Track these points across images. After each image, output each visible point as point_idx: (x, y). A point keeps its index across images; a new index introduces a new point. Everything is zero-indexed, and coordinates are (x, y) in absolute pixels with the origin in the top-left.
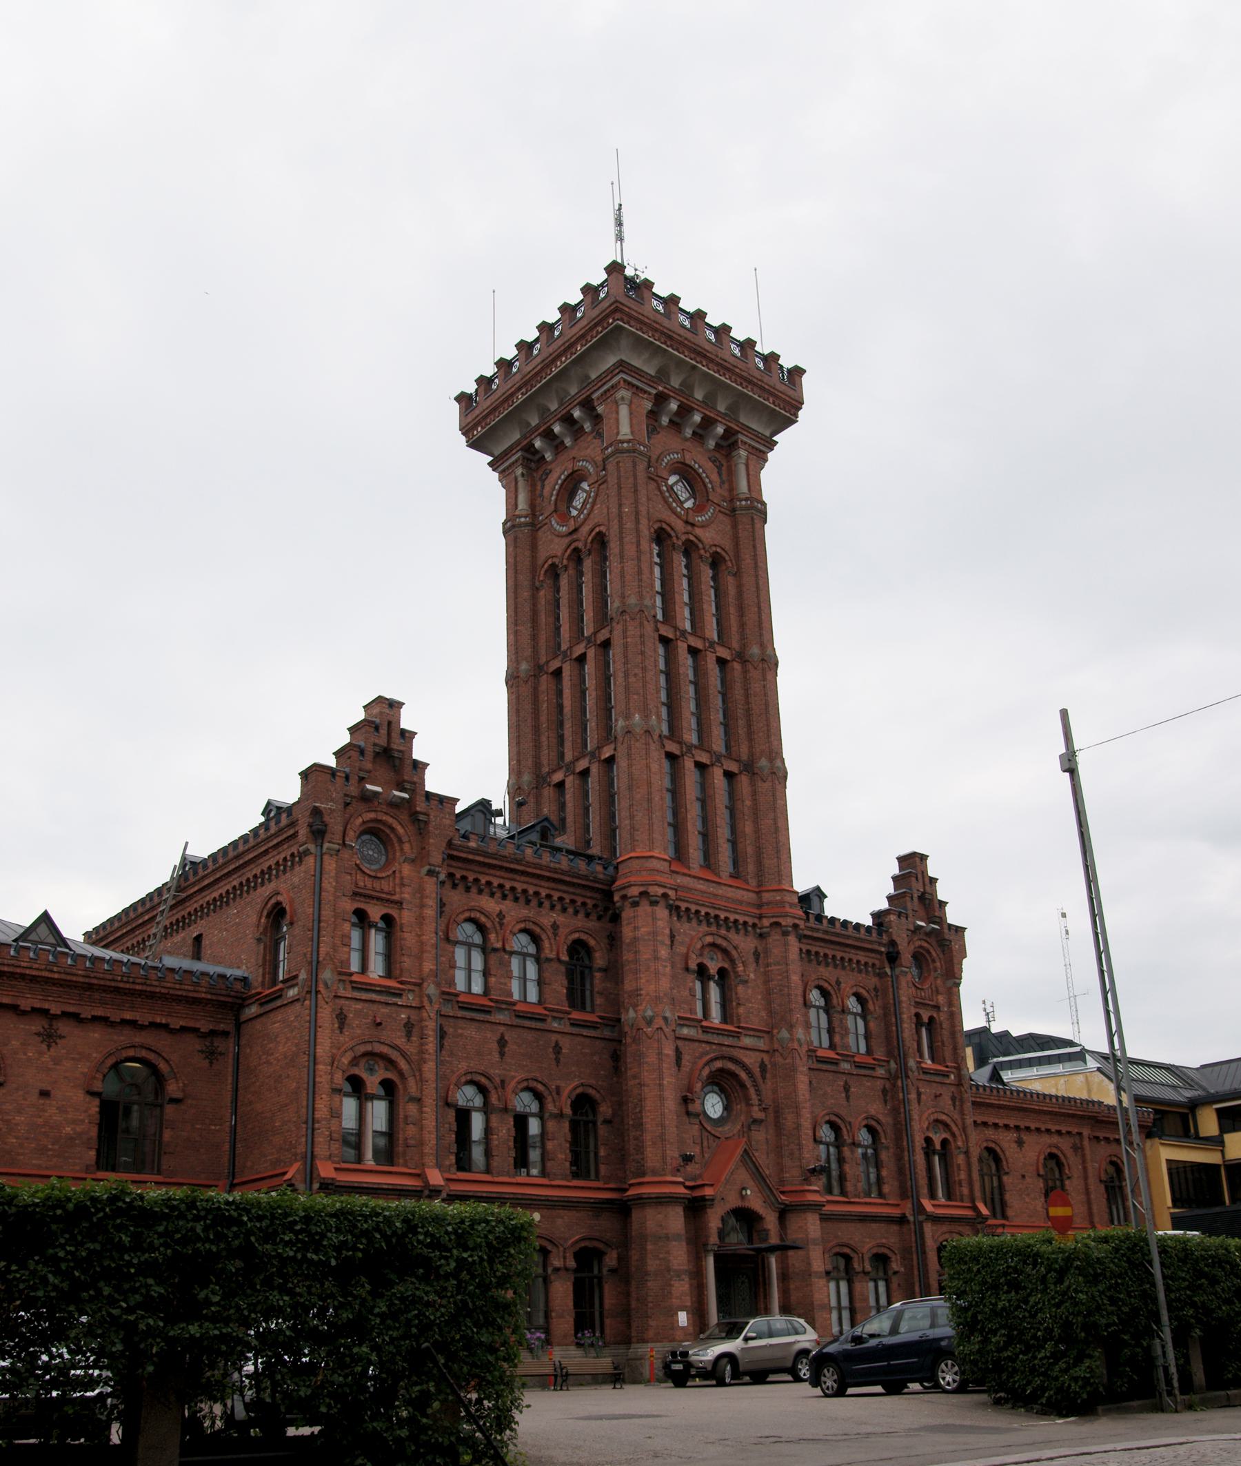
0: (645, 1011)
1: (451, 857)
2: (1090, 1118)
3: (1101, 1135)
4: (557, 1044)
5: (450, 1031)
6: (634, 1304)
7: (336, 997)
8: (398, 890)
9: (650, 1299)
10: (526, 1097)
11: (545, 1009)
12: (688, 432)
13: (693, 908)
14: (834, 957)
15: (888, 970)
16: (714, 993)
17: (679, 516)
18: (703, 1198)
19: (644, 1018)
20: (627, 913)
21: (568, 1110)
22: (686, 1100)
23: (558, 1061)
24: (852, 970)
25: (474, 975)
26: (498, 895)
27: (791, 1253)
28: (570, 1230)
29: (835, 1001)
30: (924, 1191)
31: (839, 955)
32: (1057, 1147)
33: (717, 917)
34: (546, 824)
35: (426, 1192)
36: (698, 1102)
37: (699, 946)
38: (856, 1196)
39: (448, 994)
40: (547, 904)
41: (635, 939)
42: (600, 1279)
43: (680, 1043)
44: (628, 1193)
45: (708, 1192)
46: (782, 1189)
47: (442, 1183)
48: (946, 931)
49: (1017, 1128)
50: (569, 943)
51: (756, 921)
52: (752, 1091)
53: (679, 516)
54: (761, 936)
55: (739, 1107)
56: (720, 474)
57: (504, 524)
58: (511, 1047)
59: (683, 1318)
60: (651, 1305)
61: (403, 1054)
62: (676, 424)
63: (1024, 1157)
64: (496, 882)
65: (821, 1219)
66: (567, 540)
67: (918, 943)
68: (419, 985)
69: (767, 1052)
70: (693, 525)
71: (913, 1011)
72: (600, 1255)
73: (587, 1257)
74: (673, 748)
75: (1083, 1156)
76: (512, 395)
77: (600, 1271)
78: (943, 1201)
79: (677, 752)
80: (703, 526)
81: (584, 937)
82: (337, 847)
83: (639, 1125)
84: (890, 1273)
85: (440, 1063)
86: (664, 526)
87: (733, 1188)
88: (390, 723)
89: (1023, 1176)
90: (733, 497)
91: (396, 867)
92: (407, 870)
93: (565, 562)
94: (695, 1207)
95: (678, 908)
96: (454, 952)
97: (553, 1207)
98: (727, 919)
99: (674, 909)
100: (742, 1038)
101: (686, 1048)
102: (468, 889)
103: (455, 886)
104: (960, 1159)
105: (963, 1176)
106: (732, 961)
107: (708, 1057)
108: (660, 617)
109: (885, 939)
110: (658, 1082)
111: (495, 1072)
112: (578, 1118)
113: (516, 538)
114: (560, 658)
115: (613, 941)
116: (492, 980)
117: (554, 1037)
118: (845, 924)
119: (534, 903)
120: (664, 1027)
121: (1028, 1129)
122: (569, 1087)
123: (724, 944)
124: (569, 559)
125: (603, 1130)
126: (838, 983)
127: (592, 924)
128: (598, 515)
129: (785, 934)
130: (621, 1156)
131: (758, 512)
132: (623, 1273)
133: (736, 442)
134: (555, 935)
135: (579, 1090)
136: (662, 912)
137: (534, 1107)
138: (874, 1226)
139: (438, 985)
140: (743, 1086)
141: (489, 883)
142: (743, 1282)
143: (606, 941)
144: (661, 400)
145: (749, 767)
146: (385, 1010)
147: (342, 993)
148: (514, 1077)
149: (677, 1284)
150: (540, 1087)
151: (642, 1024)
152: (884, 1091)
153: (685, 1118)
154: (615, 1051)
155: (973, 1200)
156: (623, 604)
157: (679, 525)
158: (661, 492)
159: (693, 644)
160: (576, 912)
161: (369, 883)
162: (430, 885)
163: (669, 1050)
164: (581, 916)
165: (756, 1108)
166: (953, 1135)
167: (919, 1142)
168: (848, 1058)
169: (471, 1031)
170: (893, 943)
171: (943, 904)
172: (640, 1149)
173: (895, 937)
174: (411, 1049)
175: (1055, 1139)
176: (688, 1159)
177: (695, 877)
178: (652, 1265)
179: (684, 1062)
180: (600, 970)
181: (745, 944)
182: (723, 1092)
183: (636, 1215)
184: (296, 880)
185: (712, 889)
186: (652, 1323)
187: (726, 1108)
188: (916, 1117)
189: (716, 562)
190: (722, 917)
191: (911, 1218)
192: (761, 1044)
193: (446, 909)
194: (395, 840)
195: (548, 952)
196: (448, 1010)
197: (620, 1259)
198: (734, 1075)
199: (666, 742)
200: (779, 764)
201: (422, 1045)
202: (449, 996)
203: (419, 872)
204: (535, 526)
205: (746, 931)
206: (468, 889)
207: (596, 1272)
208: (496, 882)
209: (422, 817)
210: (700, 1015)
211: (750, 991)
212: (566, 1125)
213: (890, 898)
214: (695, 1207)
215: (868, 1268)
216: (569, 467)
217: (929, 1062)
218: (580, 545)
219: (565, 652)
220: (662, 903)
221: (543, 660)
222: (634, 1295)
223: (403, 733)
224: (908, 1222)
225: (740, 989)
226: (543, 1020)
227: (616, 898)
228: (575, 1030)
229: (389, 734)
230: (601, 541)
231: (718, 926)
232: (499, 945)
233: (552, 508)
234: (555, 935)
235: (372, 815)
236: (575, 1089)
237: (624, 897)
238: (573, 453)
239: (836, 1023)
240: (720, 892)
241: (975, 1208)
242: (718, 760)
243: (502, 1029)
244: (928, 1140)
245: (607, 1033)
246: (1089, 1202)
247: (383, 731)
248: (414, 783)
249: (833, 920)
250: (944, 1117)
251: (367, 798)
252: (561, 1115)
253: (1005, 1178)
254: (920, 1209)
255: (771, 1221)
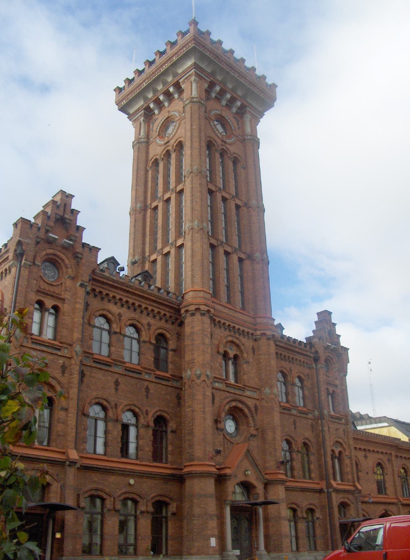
0: (196, 371)
1: (94, 280)
2: (396, 446)
3: (399, 455)
4: (147, 387)
5: (87, 373)
6: (185, 533)
7: (22, 346)
8: (63, 293)
9: (195, 530)
10: (129, 415)
11: (142, 367)
12: (224, 103)
13: (222, 321)
14: (289, 357)
15: (314, 366)
16: (231, 368)
17: (219, 138)
18: (225, 475)
19: (196, 375)
20: (188, 320)
21: (152, 424)
22: (216, 421)
23: (147, 396)
24: (297, 365)
25: (103, 345)
26: (119, 304)
27: (270, 506)
28: (151, 490)
29: (289, 379)
30: (331, 476)
31: (291, 356)
32: (381, 460)
33: (234, 327)
34: (146, 274)
35: (68, 463)
36: (223, 423)
37: (225, 341)
38: (300, 478)
39: (88, 353)
40: (145, 312)
41: (192, 333)
42: (166, 518)
43: (214, 391)
44: (184, 471)
45: (228, 471)
46: (266, 472)
47: (77, 458)
48: (340, 349)
49: (365, 450)
50: (156, 334)
51: (254, 332)
52: (250, 419)
53: (219, 138)
54: (256, 340)
55: (243, 427)
56: (238, 124)
57: (133, 142)
58: (121, 387)
59: (213, 542)
60: (195, 534)
61: (59, 383)
62: (218, 99)
63: (369, 463)
64: (118, 297)
65: (286, 490)
66: (163, 147)
67: (328, 354)
68: (71, 345)
69: (258, 400)
70: (225, 142)
71: (326, 386)
72: (167, 504)
73: (160, 505)
74: (214, 242)
75: (392, 464)
76: (141, 84)
77: (166, 513)
78: (340, 482)
79: (216, 244)
80: (230, 144)
81: (164, 332)
82: (29, 263)
83: (191, 433)
84: (315, 518)
85: (80, 391)
86: (212, 140)
87: (240, 469)
88: (65, 205)
89: (367, 473)
90: (244, 134)
91: (63, 281)
92: (69, 283)
93: (162, 157)
94: (221, 479)
95: (214, 320)
96: (92, 331)
97: (142, 477)
98: (239, 329)
99: (213, 320)
100: (246, 391)
101: (218, 394)
102: (102, 299)
103: (95, 296)
104: (347, 461)
105: (349, 469)
106: (241, 351)
107: (228, 400)
108: (210, 234)
109: (313, 350)
110: (200, 410)
111: (113, 400)
112: (157, 428)
113: (139, 148)
114: (157, 201)
115: (180, 336)
116: (113, 349)
117: (146, 383)
118: (295, 340)
119: (138, 311)
120: (206, 380)
121: (369, 450)
122: (153, 412)
123: (238, 342)
124: (164, 155)
125: (170, 436)
126: (291, 370)
127: (169, 326)
128: (181, 132)
129: (269, 339)
130: (180, 450)
131: (256, 143)
132: (178, 515)
133: (246, 111)
134: (149, 329)
135: (158, 413)
136: (207, 320)
137: (133, 421)
138: (308, 494)
139: (82, 346)
140: (246, 417)
141: (114, 297)
142: (245, 522)
143: (176, 336)
144: (212, 85)
145: (250, 257)
146: (51, 357)
147: (25, 344)
148: (123, 403)
149: (210, 522)
150: (137, 410)
151: (195, 378)
152: (312, 426)
153: (216, 431)
154: (178, 394)
155: (354, 482)
156: (192, 169)
157: (219, 142)
158: (211, 125)
159: (224, 195)
160: (161, 319)
161: (47, 287)
162: (81, 293)
163: (209, 393)
164: (163, 321)
165: (252, 429)
166: (344, 449)
167: (329, 453)
168: (296, 407)
169: (99, 375)
170: (316, 352)
171: (339, 336)
172: (191, 446)
173: (318, 350)
174: (64, 380)
175: (380, 456)
176: (218, 452)
177: (223, 306)
178: (197, 511)
179: (216, 401)
180: (172, 350)
181: (247, 343)
182: (235, 419)
183: (188, 483)
184: (6, 283)
185: (232, 313)
186: (196, 544)
187: (236, 429)
188: (328, 439)
189: (235, 161)
190: (237, 328)
191: (326, 490)
192: (255, 395)
193: (90, 308)
194: (63, 266)
195: (144, 337)
196: (89, 362)
197: (177, 507)
198: (241, 410)
199: (210, 238)
200: (265, 256)
201: (70, 378)
202: (88, 354)
203: (76, 285)
204: (148, 143)
205: (248, 335)
206: (102, 299)
207: (164, 514)
208: (118, 297)
209: (79, 255)
210: (224, 377)
211: (250, 368)
212: (151, 432)
213: (314, 331)
214: (221, 479)
215: (305, 516)
216: (166, 115)
217: (333, 412)
218: (170, 148)
219: (160, 197)
220: (207, 315)
221: (147, 254)
222: (185, 528)
223: (73, 211)
224: (324, 492)
225: (245, 366)
226: (140, 373)
227: (183, 311)
228: (158, 381)
229: (64, 211)
230: (180, 145)
231: (235, 332)
232: (118, 330)
233: (157, 133)
234: (149, 329)
235: (52, 251)
236: (156, 412)
237: (187, 311)
238: (167, 109)
239: (289, 390)
240: (236, 315)
241: (355, 486)
242: (236, 251)
243: (117, 376)
244: (333, 451)
245: (175, 384)
246: (395, 486)
247: (62, 208)
248: (76, 237)
249: (289, 338)
250: (340, 440)
251: (50, 242)
252: (148, 426)
253: (360, 474)
254: (329, 485)
255: (260, 488)
